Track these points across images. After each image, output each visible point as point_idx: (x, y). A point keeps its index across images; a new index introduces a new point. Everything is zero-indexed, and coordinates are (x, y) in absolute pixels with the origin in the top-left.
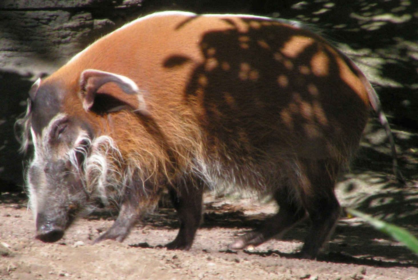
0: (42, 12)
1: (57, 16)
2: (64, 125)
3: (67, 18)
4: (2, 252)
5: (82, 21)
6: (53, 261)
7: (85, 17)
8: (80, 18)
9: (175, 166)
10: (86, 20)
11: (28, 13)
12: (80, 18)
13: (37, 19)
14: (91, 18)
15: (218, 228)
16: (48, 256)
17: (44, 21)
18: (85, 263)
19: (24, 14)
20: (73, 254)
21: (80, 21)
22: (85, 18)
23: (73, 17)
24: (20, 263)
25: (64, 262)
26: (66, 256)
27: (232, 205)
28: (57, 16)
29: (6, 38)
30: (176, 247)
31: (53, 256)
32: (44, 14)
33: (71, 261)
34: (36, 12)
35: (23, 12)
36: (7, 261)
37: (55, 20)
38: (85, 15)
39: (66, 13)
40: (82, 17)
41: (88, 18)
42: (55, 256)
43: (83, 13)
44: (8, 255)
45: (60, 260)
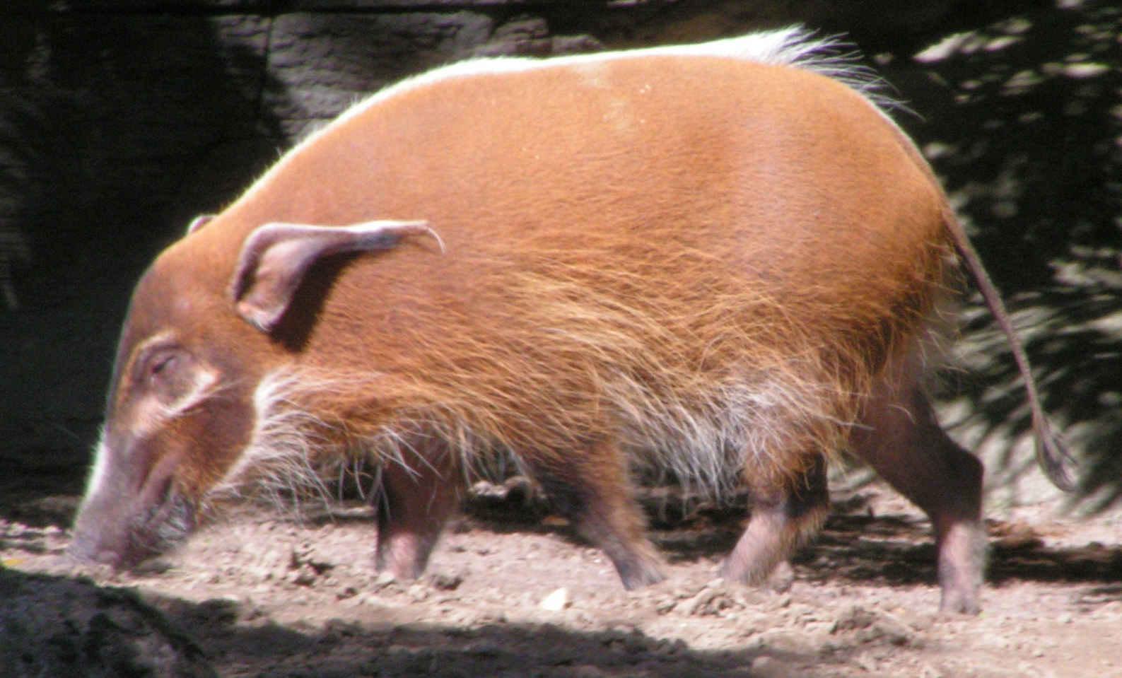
0: (419, 17)
1: (460, 27)
2: (169, 354)
3: (485, 32)
4: (893, 635)
5: (523, 41)
6: (1024, 658)
7: (531, 29)
8: (517, 31)
9: (446, 457)
10: (533, 38)
11: (385, 19)
12: (517, 31)
13: (405, 35)
14: (545, 31)
15: (1017, 582)
16: (1007, 646)
17: (424, 41)
18: (1111, 665)
19: (373, 22)
20: (1072, 640)
21: (519, 39)
22: (531, 32)
23: (501, 30)
24: (950, 666)
25: (1053, 661)
26: (1056, 646)
27: (1002, 523)
28: (460, 27)
29: (328, 84)
30: (433, 665)
31: (1019, 647)
32: (426, 22)
33: (1071, 659)
34: (404, 15)
35: (371, 17)
36: (913, 660)
37: (453, 36)
38: (530, 24)
39: (483, 19)
40: (523, 31)
41: (538, 33)
42: (1025, 647)
43: (526, 19)
44: (907, 644)
45: (1041, 656)
